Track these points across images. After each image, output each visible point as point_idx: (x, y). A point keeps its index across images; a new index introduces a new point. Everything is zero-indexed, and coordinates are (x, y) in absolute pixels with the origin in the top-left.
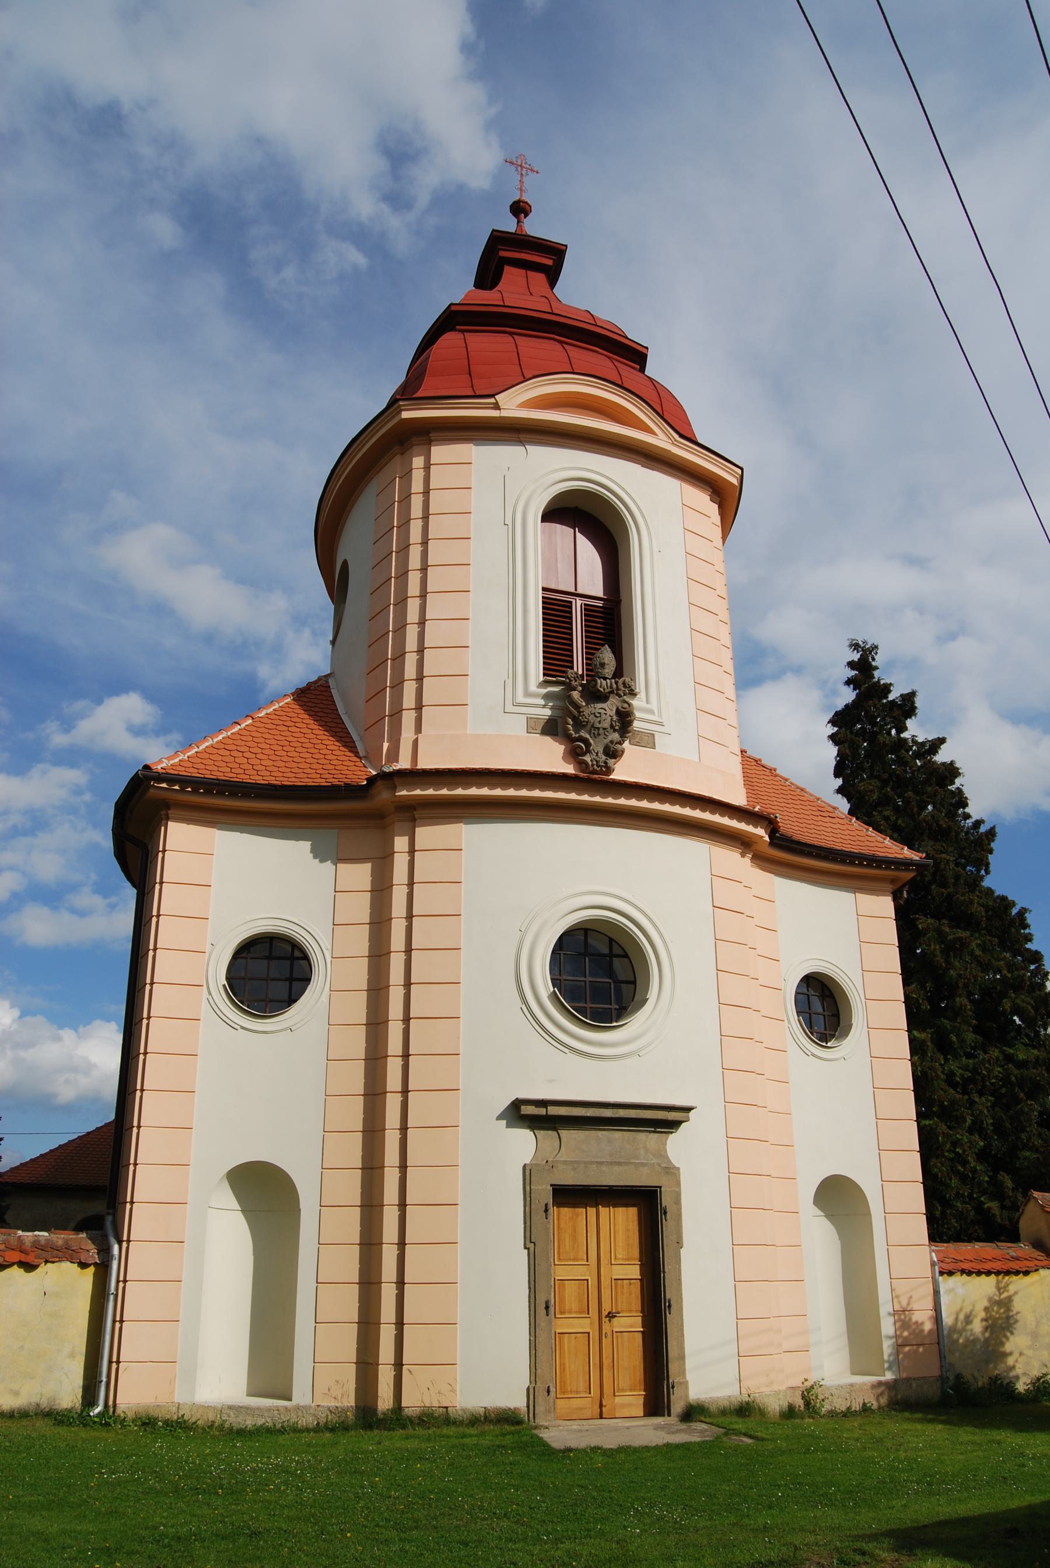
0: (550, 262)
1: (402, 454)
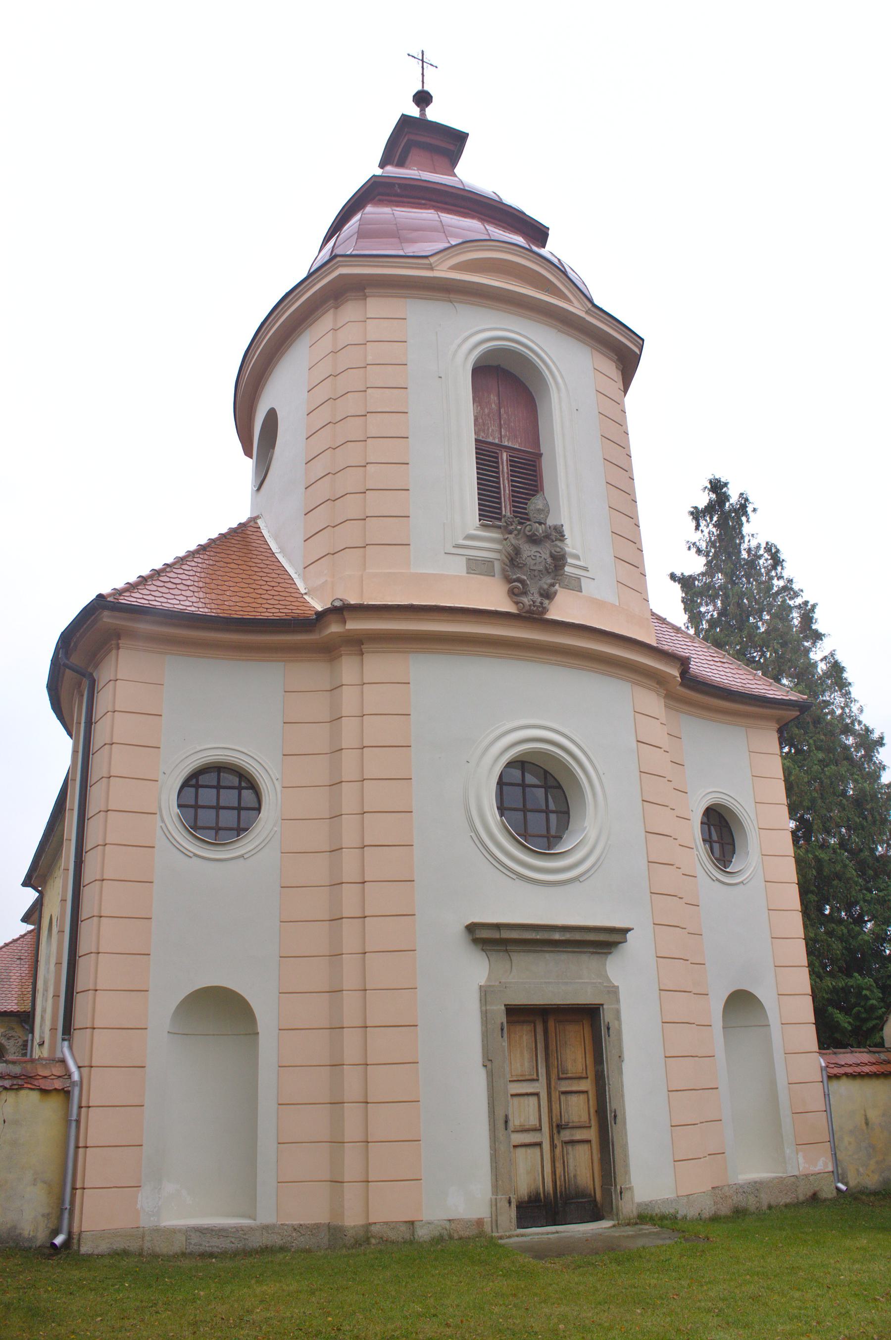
0: (451, 147)
1: (336, 308)
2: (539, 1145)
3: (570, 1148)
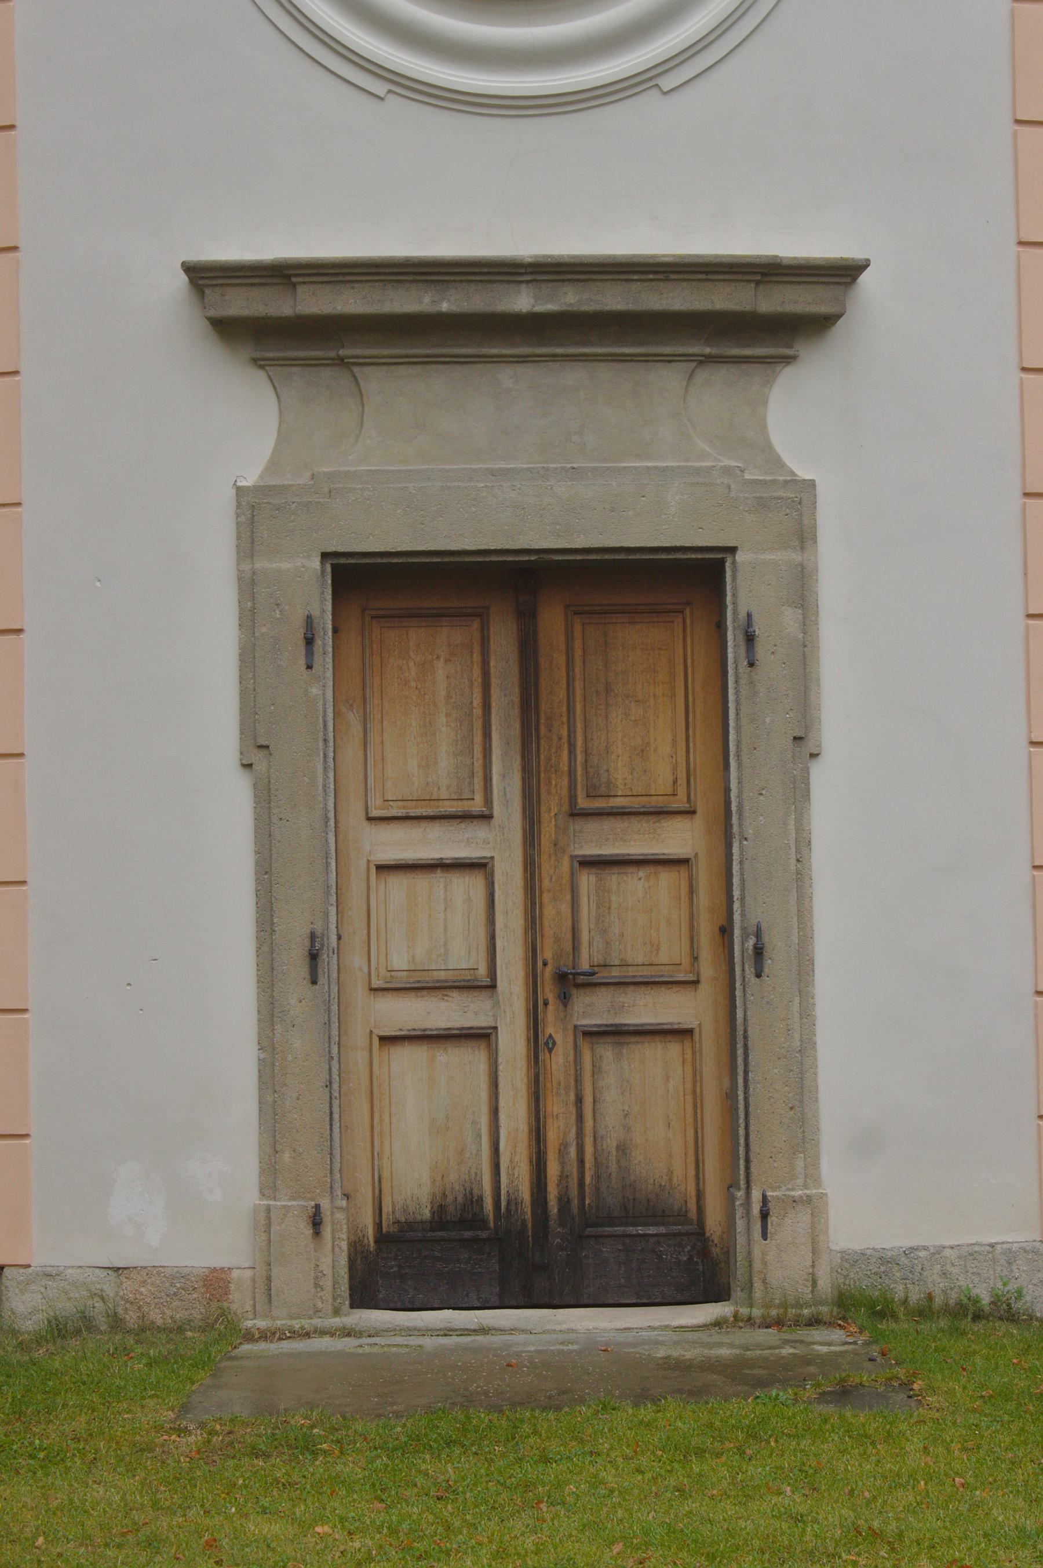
2: (482, 1036)
3: (607, 1052)
